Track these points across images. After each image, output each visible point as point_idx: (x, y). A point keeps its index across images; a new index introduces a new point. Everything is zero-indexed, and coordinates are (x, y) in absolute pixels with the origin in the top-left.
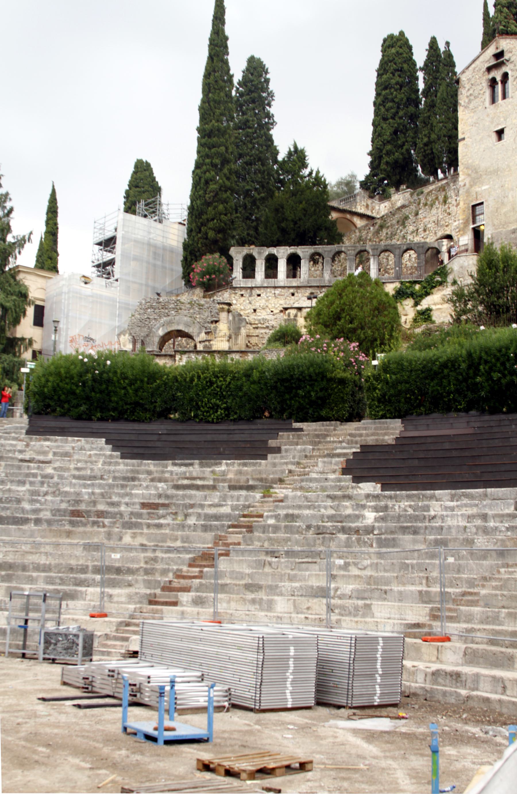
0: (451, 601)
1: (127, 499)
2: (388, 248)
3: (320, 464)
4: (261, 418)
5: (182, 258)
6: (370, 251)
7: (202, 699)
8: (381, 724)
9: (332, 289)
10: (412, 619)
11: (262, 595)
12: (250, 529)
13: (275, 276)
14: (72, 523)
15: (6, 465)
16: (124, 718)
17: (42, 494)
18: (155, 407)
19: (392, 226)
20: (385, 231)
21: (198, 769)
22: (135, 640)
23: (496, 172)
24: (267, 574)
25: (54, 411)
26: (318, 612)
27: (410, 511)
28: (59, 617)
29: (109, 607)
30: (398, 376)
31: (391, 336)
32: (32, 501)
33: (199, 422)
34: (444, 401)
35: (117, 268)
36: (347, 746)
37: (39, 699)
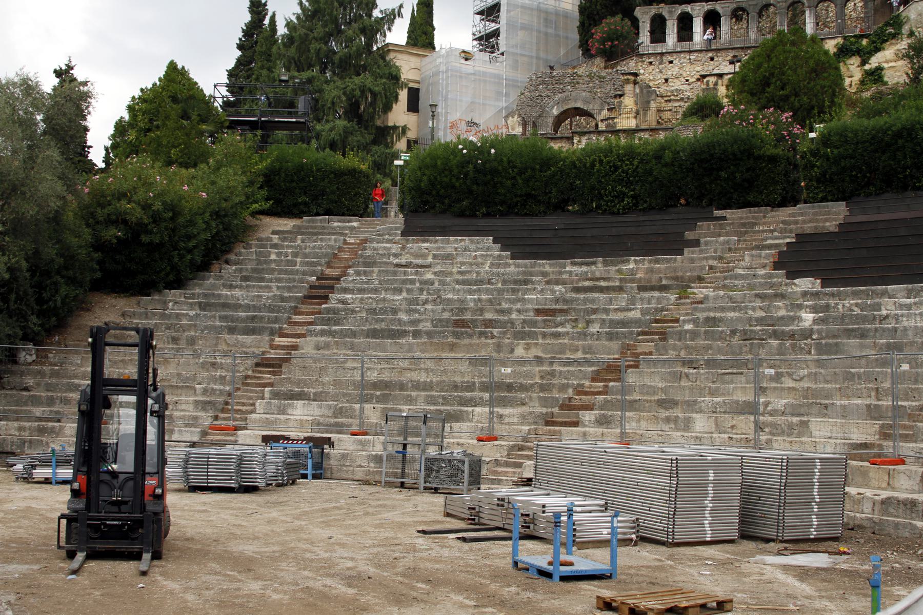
0: (906, 417)
1: (519, 306)
3: (747, 258)
4: (675, 206)
5: (578, 24)
7: (605, 531)
8: (819, 560)
9: (759, 49)
10: (858, 437)
11: (678, 412)
12: (663, 336)
13: (690, 39)
14: (456, 335)
15: (379, 271)
16: (515, 552)
17: (421, 303)
18: (550, 198)
21: (598, 608)
22: (529, 466)
24: (684, 388)
25: (433, 207)
26: (744, 431)
27: (857, 311)
28: (442, 442)
29: (499, 429)
30: (841, 150)
31: (833, 103)
32: (409, 312)
33: (602, 214)
35: (502, 40)
36: (775, 585)
37: (419, 532)
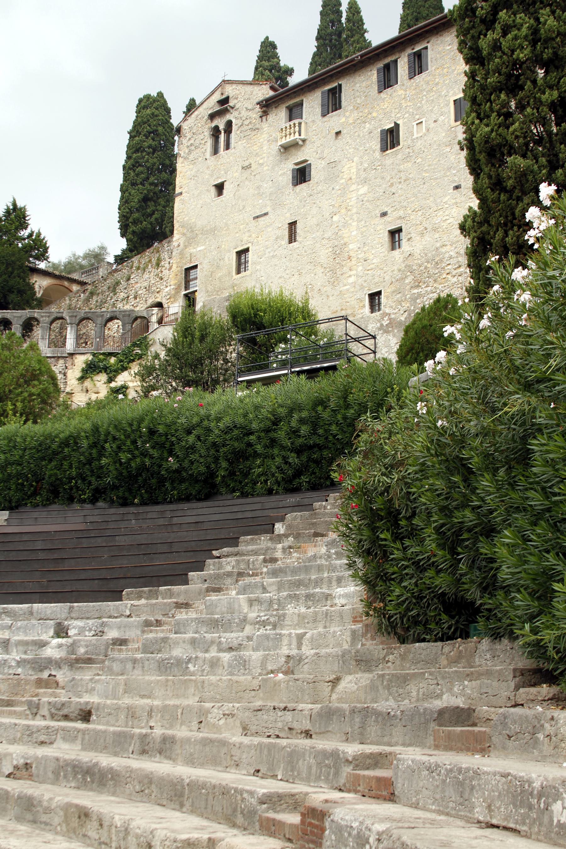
2: (89, 315)
6: (68, 318)
19: (103, 292)
20: (95, 298)
23: (212, 231)
34: (65, 489)
